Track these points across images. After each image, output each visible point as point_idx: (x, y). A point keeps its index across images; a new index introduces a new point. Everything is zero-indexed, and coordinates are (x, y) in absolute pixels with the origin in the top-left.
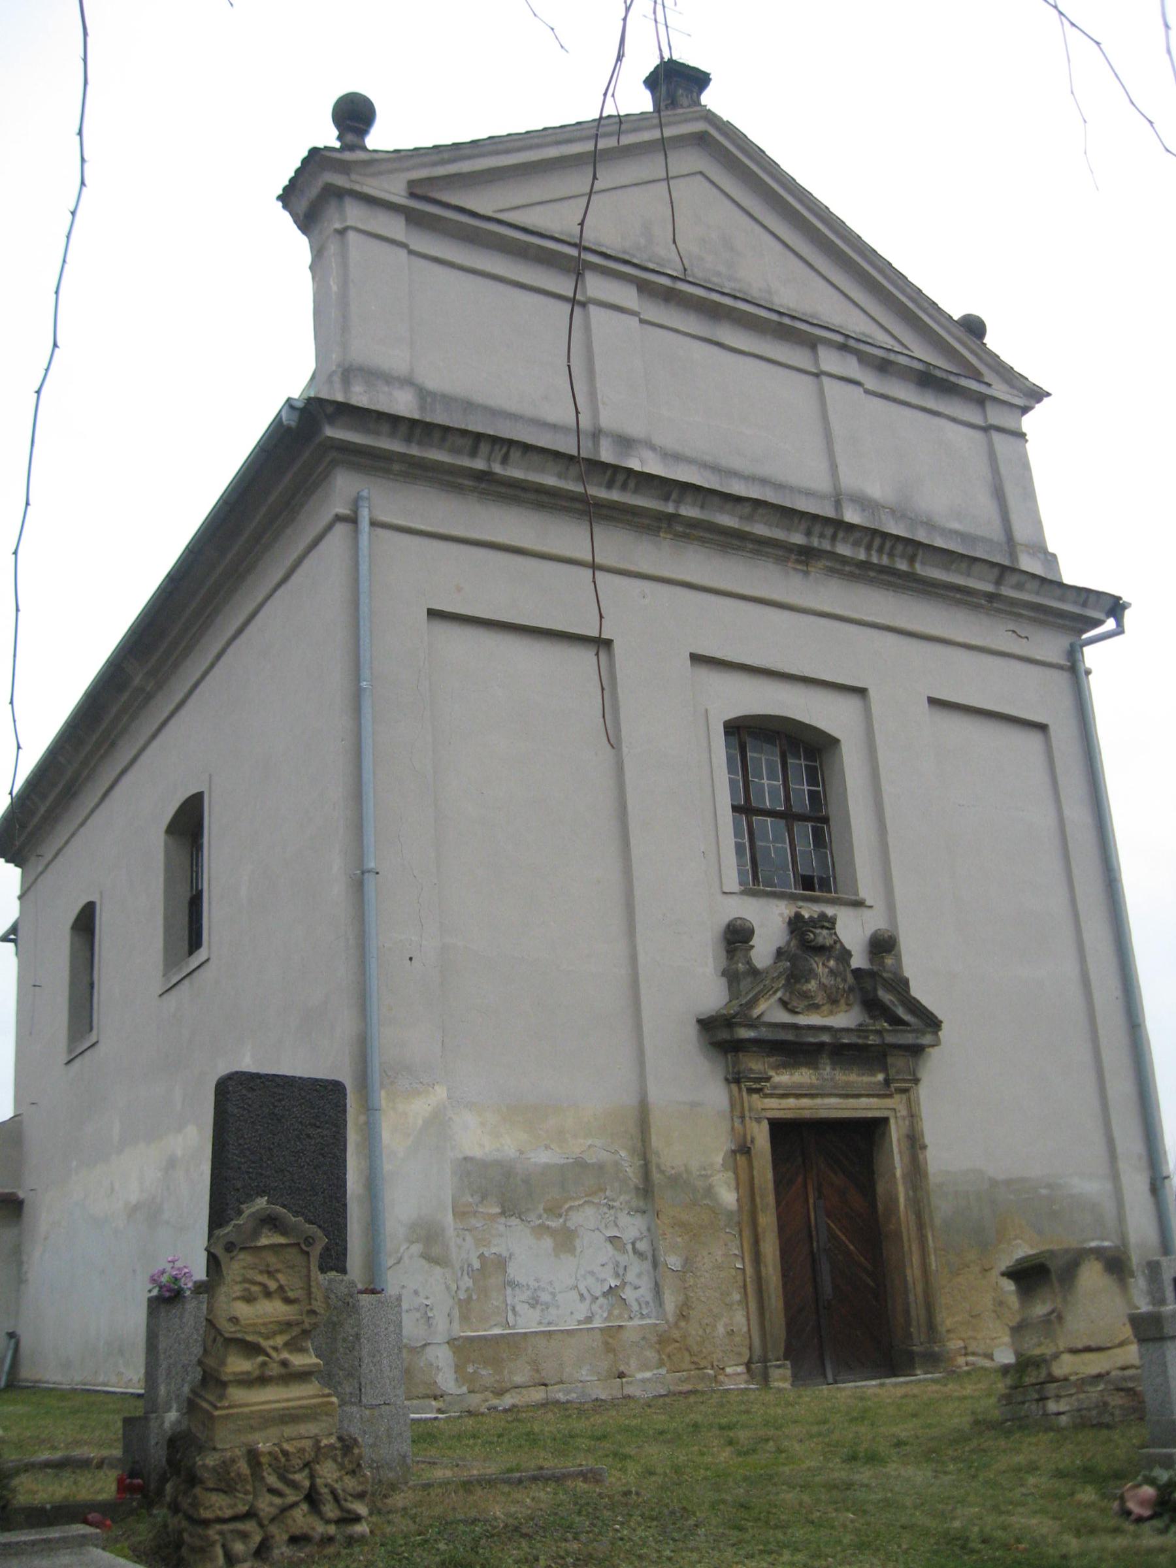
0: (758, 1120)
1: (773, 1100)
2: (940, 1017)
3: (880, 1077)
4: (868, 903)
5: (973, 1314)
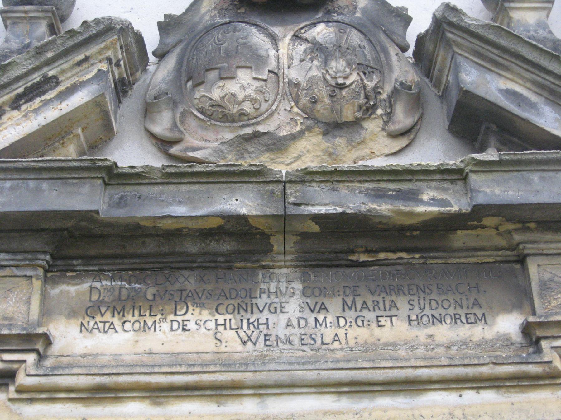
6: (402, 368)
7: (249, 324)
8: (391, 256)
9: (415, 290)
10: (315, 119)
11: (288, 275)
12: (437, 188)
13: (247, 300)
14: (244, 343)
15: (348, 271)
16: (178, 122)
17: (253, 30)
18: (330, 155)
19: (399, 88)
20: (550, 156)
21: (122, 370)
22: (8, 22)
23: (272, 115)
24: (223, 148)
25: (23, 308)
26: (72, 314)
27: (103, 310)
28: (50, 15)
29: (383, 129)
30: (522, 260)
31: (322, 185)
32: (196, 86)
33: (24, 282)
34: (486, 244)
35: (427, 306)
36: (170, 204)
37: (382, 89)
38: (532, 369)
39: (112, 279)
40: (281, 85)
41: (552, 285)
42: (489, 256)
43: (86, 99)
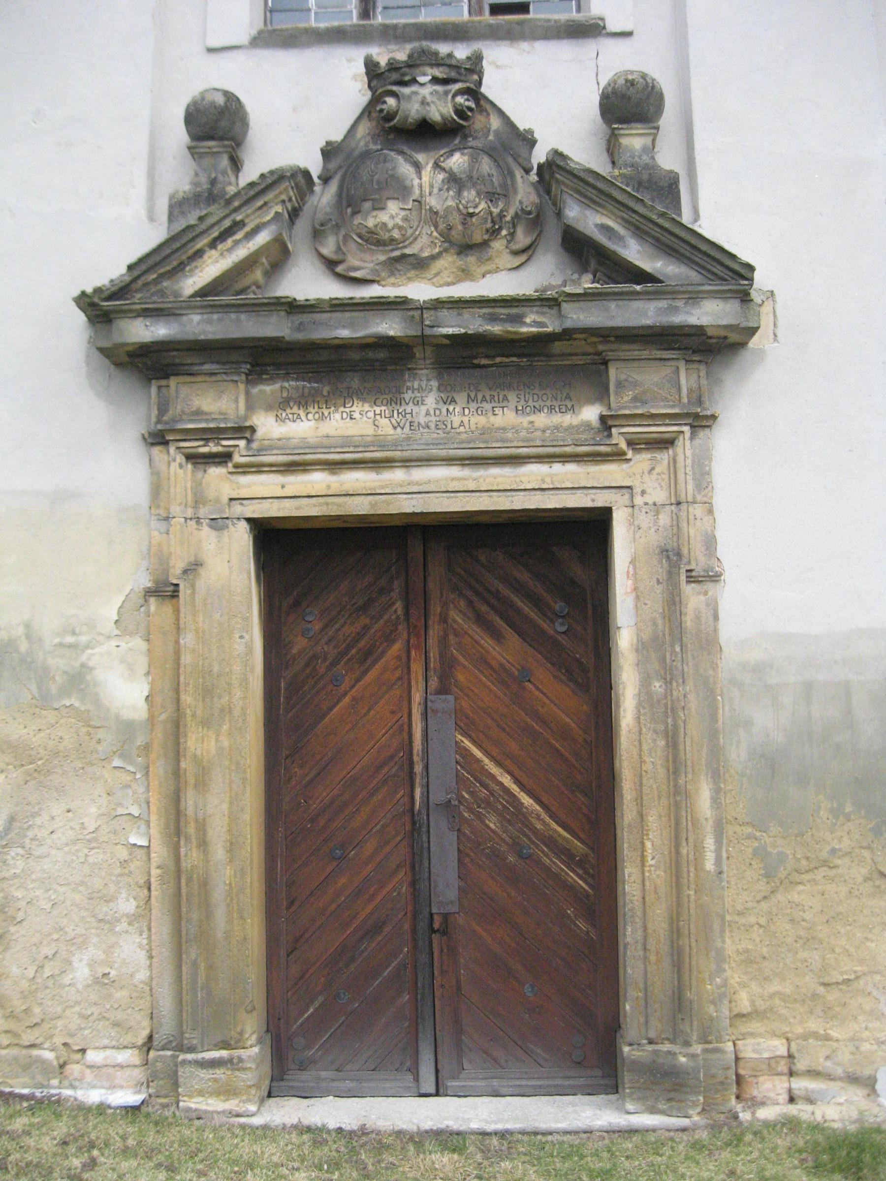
0: (218, 524)
1: (263, 478)
2: (745, 256)
3: (591, 413)
4: (613, 25)
5: (827, 980)
6: (508, 447)
7: (398, 413)
8: (506, 360)
9: (522, 387)
10: (450, 242)
11: (427, 375)
12: (537, 312)
13: (398, 396)
14: (395, 428)
15: (471, 371)
16: (341, 243)
17: (400, 159)
18: (463, 271)
19: (520, 213)
20: (624, 289)
21: (307, 451)
22: (196, 156)
23: (416, 239)
24: (377, 267)
25: (234, 406)
26: (269, 408)
27: (291, 404)
28: (231, 150)
29: (507, 247)
30: (605, 363)
31: (450, 311)
32: (354, 213)
33: (231, 385)
34: (578, 351)
35: (531, 399)
36: (337, 328)
37: (507, 212)
38: (602, 449)
39: (297, 380)
40: (423, 211)
41: (626, 384)
42: (580, 360)
43: (268, 239)
